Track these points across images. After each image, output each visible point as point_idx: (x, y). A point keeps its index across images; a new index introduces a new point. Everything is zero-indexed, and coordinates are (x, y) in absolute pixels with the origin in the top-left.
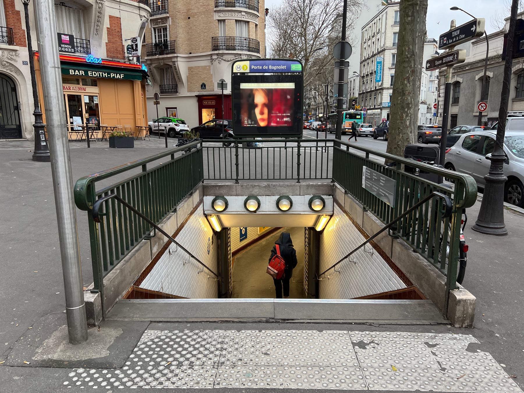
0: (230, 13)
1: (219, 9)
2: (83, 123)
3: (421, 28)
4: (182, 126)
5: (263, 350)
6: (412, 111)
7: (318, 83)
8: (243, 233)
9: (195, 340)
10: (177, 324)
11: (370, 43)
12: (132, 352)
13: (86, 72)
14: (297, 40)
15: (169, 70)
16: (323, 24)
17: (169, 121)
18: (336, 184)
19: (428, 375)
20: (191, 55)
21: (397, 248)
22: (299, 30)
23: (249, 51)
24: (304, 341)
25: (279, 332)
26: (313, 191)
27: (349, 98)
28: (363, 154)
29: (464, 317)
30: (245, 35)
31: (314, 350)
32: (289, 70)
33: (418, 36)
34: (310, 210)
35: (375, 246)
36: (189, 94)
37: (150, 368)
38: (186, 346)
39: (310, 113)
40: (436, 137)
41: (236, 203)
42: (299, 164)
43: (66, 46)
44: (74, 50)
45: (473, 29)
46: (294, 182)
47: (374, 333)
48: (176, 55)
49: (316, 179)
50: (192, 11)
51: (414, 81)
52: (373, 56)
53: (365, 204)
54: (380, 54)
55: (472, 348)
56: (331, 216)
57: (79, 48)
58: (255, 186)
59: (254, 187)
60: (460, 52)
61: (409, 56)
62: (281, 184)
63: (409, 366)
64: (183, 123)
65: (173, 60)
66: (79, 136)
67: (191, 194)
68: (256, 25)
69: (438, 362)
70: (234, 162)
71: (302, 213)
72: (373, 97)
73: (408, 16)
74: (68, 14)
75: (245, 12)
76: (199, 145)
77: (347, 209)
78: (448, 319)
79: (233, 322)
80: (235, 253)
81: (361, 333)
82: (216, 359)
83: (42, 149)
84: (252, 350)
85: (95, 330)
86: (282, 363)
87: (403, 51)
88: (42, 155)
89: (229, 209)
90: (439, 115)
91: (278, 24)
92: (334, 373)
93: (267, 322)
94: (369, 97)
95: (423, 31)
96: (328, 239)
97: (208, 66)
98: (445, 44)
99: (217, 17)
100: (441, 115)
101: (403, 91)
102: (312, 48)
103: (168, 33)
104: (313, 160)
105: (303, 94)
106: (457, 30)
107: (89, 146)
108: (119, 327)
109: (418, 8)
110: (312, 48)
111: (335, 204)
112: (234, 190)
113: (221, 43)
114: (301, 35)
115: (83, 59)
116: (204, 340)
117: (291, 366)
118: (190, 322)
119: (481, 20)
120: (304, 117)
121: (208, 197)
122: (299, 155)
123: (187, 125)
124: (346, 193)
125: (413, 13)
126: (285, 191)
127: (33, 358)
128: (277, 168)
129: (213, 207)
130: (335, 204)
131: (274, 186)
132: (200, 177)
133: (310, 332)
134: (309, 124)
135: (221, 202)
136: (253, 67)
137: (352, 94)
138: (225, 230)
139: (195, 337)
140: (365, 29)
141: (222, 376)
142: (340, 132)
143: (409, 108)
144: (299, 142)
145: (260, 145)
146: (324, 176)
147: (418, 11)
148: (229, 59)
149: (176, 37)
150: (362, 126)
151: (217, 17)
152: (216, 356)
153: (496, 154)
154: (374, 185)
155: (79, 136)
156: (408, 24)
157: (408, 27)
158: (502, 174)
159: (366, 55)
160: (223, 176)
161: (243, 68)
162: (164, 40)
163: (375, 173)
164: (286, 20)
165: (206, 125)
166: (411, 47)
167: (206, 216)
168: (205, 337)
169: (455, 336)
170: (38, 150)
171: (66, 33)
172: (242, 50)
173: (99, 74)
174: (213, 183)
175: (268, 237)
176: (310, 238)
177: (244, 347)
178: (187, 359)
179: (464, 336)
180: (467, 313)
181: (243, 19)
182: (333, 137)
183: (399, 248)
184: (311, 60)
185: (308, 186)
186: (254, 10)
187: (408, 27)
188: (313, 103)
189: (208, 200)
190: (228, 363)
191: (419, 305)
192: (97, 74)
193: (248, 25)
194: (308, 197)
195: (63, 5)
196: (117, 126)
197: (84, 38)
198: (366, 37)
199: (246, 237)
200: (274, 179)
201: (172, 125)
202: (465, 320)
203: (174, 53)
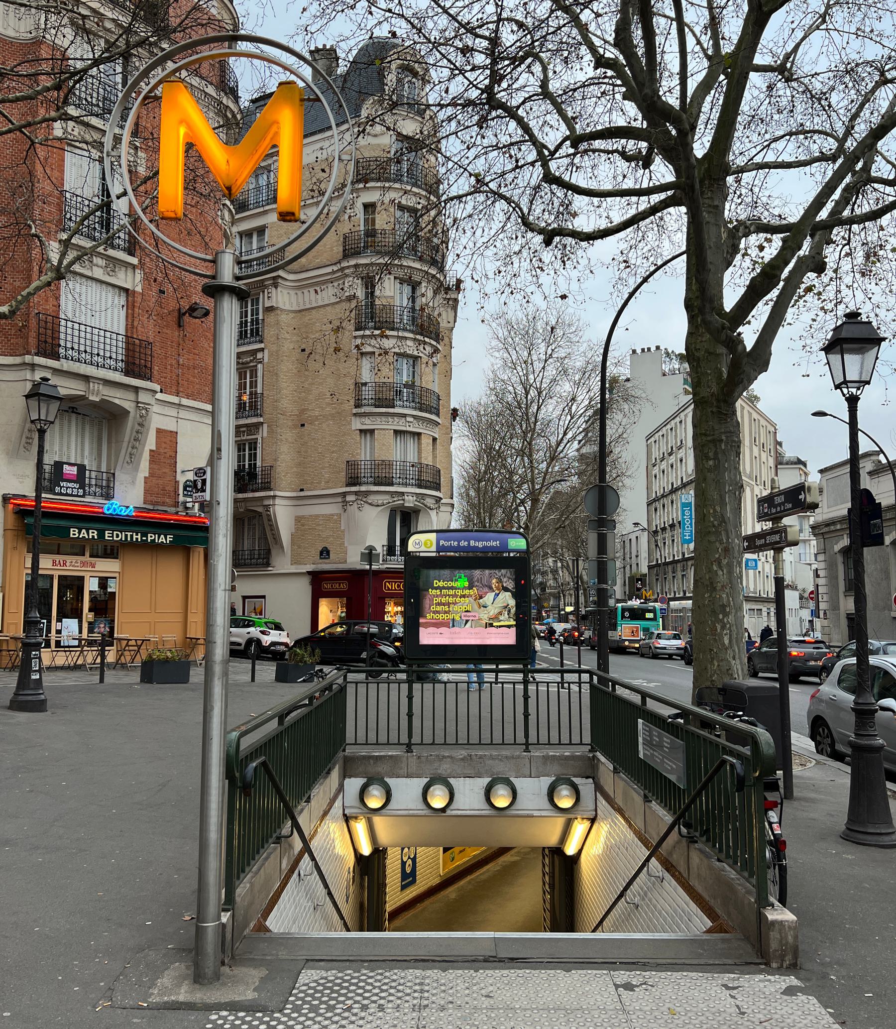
0: (384, 419)
1: (362, 410)
2: (80, 632)
3: (733, 477)
4: (274, 635)
5: (483, 992)
6: (731, 618)
7: (559, 543)
9: (380, 981)
10: (348, 964)
11: (664, 465)
12: (291, 995)
13: (101, 534)
14: (515, 462)
15: (256, 521)
16: (565, 434)
17: (249, 624)
18: (598, 754)
19: (720, 1018)
20: (302, 494)
21: (695, 858)
22: (517, 443)
23: (420, 486)
24: (543, 982)
25: (506, 972)
26: (556, 768)
27: (628, 575)
28: (636, 699)
29: (782, 950)
30: (412, 457)
31: (558, 992)
33: (729, 490)
34: (552, 808)
35: (668, 866)
36: (293, 569)
37: (322, 1011)
38: (369, 988)
39: (545, 605)
40: (813, 663)
42: (526, 715)
43: (69, 485)
44: (84, 491)
45: (802, 497)
46: (518, 751)
47: (648, 973)
48: (272, 493)
49: (560, 744)
50: (309, 413)
51: (730, 566)
52: (674, 491)
53: (645, 788)
55: (790, 991)
56: (593, 821)
57: (93, 489)
58: (444, 757)
60: (788, 529)
61: (716, 523)
63: (695, 1009)
64: (278, 627)
65: (266, 502)
66: (70, 659)
67: (328, 773)
68: (435, 439)
69: (738, 1006)
71: (536, 813)
72: (679, 574)
73: (708, 458)
74: (80, 424)
75: (413, 416)
76: (340, 681)
77: (619, 801)
78: (762, 958)
79: (433, 961)
81: (628, 973)
82: (415, 1002)
83: (32, 686)
84: (467, 992)
85: (226, 970)
86: (511, 1006)
87: (705, 515)
88: (30, 698)
89: (393, 805)
90: (822, 615)
91: (477, 431)
92: (587, 1016)
93: (485, 961)
94: (670, 575)
95: (737, 483)
96: (588, 867)
97: (337, 515)
98: (766, 514)
99: (357, 424)
100: (825, 614)
101: (712, 583)
102: (544, 478)
103: (259, 452)
105: (530, 564)
106: (781, 494)
107: (102, 680)
108: (261, 965)
109: (723, 447)
110: (544, 478)
112: (404, 765)
113: (364, 472)
114: (521, 453)
115: (99, 508)
116: (394, 981)
117: (525, 1010)
118: (367, 961)
119: (811, 485)
121: (352, 779)
122: (526, 697)
123: (285, 633)
124: (615, 771)
125: (716, 453)
126: (501, 768)
127: (150, 1000)
128: (486, 723)
131: (481, 757)
132: (338, 739)
133: (553, 971)
135: (377, 789)
136: (442, 542)
137: (634, 566)
138: (379, 853)
139: (379, 977)
140: (652, 439)
141: (427, 1019)
142: (607, 648)
143: (726, 615)
144: (525, 672)
147: (724, 452)
148: (380, 502)
149: (275, 460)
150: (659, 636)
151: (357, 424)
152: (414, 998)
153: (860, 701)
154: (667, 759)
155: (70, 659)
156: (709, 471)
157: (710, 476)
158: (876, 735)
159: (658, 488)
161: (426, 544)
162: (250, 465)
163: (656, 731)
164: (490, 425)
165: (327, 632)
166: (718, 509)
167: (347, 819)
168: (395, 977)
169: (769, 977)
170: (24, 690)
171: (73, 462)
172: (406, 485)
173: (126, 536)
174: (363, 752)
175: (462, 883)
176: (553, 873)
177: (454, 989)
178: (375, 1002)
179: (783, 978)
180: (787, 943)
181: (408, 429)
183: (699, 860)
184: (545, 499)
185: (546, 758)
186: (431, 413)
187: (710, 476)
188: (551, 582)
189: (353, 785)
190: (434, 1005)
191: (723, 940)
192: (122, 536)
193: (419, 439)
194: (546, 781)
195: (73, 412)
196: (147, 637)
197: (104, 469)
198: (656, 454)
199: (414, 881)
200: (480, 744)
201: (254, 631)
202: (784, 956)
203: (271, 490)
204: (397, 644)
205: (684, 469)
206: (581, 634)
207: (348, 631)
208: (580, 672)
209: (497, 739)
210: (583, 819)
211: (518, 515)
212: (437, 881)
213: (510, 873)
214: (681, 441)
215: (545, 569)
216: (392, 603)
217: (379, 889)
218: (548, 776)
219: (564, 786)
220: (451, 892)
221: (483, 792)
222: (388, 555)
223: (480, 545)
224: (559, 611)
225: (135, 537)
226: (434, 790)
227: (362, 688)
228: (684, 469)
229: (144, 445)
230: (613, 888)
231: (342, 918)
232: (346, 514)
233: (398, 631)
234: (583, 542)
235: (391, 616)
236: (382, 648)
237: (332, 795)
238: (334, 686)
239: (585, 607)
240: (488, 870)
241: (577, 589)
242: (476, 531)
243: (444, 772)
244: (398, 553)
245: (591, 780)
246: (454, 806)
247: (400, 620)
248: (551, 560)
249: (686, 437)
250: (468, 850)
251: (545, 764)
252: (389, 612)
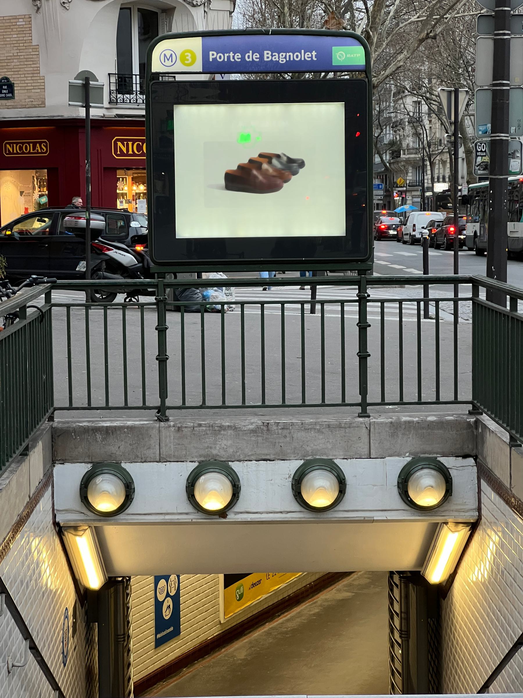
7: (425, 67)
8: (167, 614)
18: (485, 418)
32: (325, 62)
34: (407, 508)
39: (399, 181)
41: (160, 483)
42: (363, 356)
56: (474, 527)
59: (218, 430)
62: (309, 420)
67: (25, 453)
70: (152, 351)
71: (378, 516)
76: (40, 301)
80: (144, 686)
96: (464, 605)
97: (24, 17)
104: (410, 348)
105: (371, 109)
111: (483, 483)
112: (154, 442)
120: (378, 195)
121: (67, 465)
122: (363, 326)
124: (513, 442)
126: (320, 445)
129: (84, 498)
130: (483, 483)
132: (40, 399)
134: (396, 220)
136: (212, 55)
138: (116, 585)
145: (216, 295)
146: (447, 394)
160: (117, 400)
161: (183, 59)
165: (16, 228)
167: (60, 530)
174: (84, 420)
175: (257, 634)
176: (407, 612)
182: (475, 267)
188: (410, 141)
189: (69, 475)
194: (396, 464)
199: (177, 633)
204: (139, 248)
206: (460, 230)
207: (53, 227)
208: (456, 281)
209: (313, 395)
210: (457, 523)
211: (353, 16)
212: (214, 632)
213: (335, 617)
215: (400, 117)
216: (129, 179)
217: (117, 643)
218: (398, 455)
219: (426, 471)
220: (239, 650)
221: (288, 484)
222: (119, 91)
223: (281, 58)
224: (423, 191)
226: (206, 481)
227: (78, 314)
230: (507, 633)
231: (56, 687)
232: (40, 16)
233: (140, 224)
234: (467, 64)
235: (128, 202)
236: (115, 254)
237: (33, 491)
238: (29, 311)
239: (468, 183)
240: (299, 615)
241: (455, 145)
242: (275, 33)
243: (222, 453)
244: (136, 87)
245: (471, 461)
246: (239, 506)
247: (142, 207)
248: (409, 101)
250: (266, 583)
251: (393, 435)
252: (123, 195)
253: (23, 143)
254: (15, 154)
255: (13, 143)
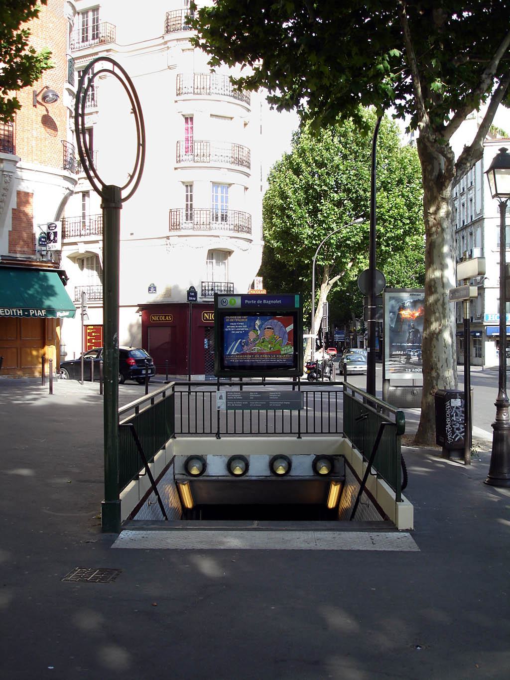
54: (476, 225)
107: (241, 389)
173: (13, 312)
205: (473, 209)
214: (471, 183)
225: (18, 312)
228: (473, 209)
229: (8, 207)
249: (475, 179)
253: (160, 316)
254: (210, 320)
255: (209, 313)
